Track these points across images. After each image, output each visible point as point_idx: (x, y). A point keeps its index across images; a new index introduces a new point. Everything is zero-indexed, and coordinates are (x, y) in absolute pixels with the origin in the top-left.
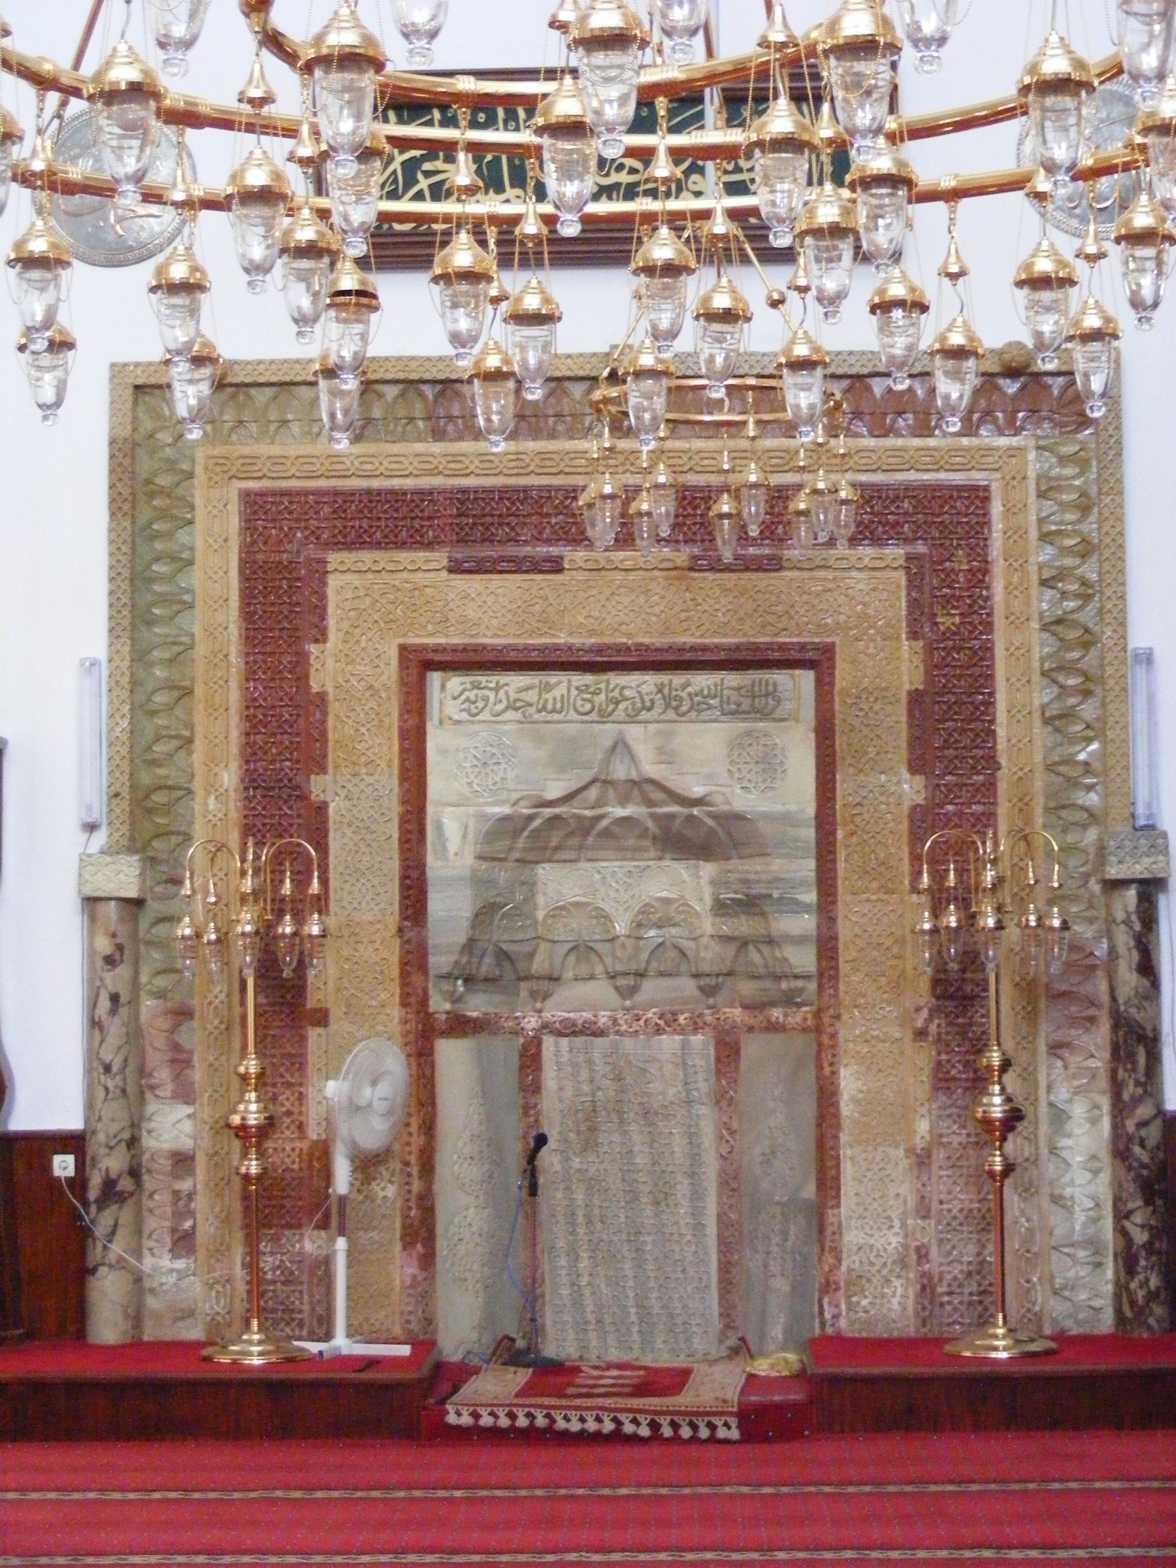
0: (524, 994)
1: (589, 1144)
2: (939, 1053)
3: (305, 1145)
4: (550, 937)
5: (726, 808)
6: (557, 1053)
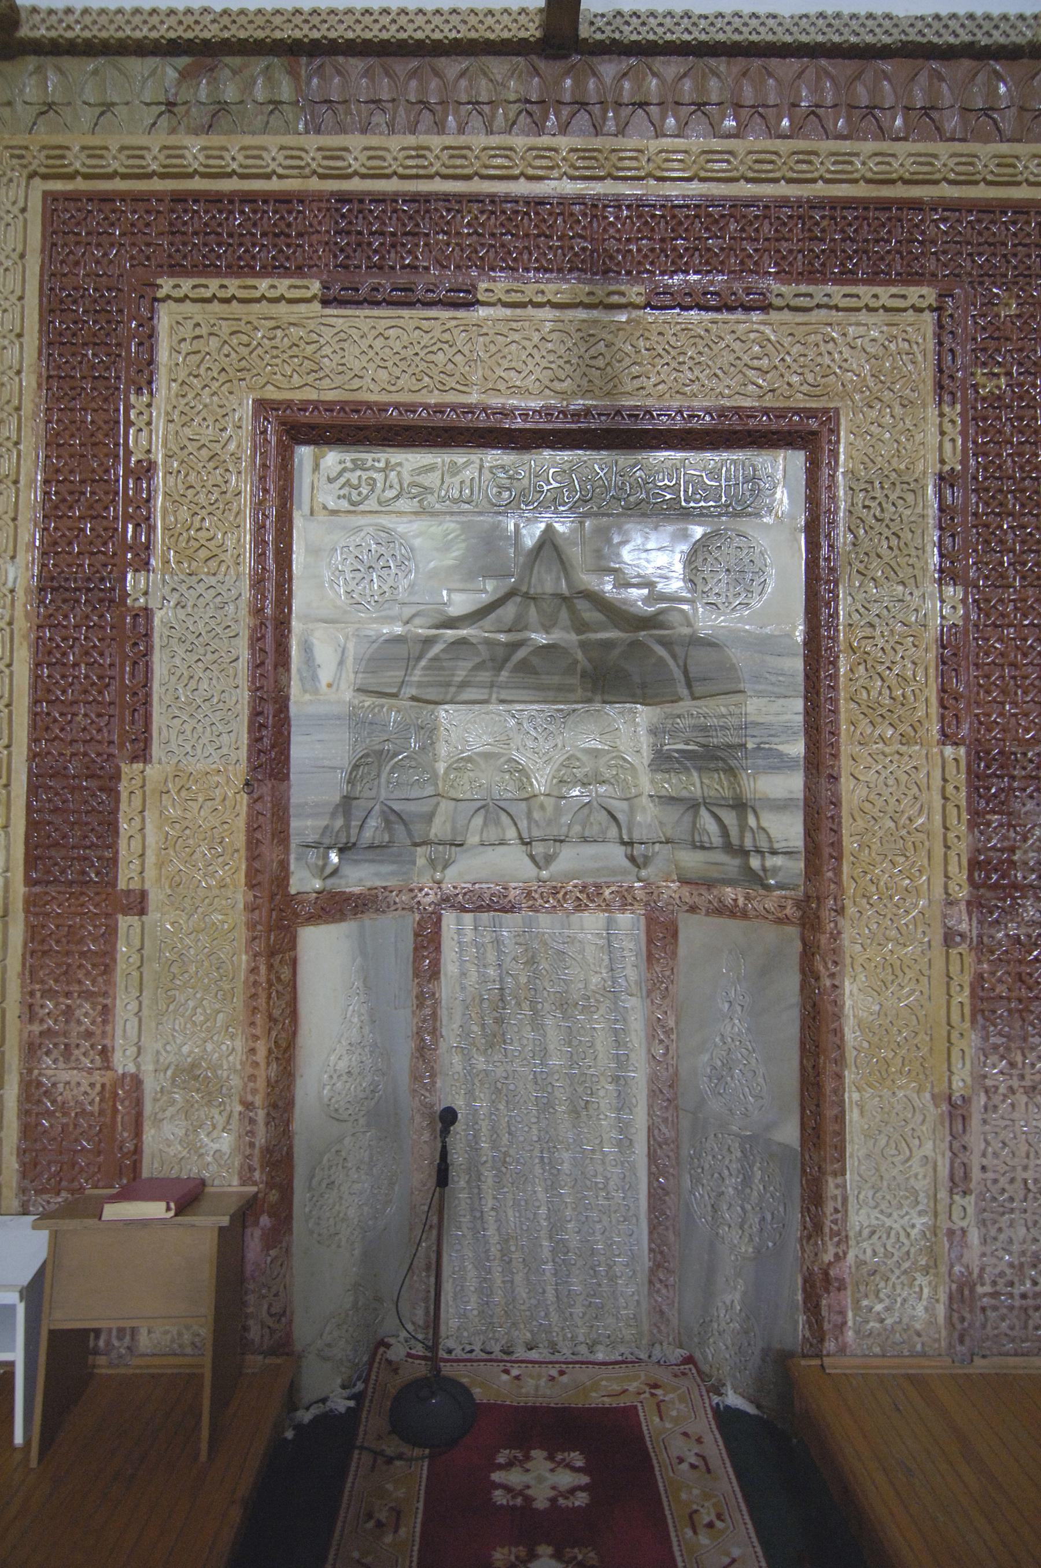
0: (421, 862)
1: (495, 1039)
2: (980, 962)
3: (108, 1077)
4: (453, 794)
5: (686, 631)
6: (459, 932)
